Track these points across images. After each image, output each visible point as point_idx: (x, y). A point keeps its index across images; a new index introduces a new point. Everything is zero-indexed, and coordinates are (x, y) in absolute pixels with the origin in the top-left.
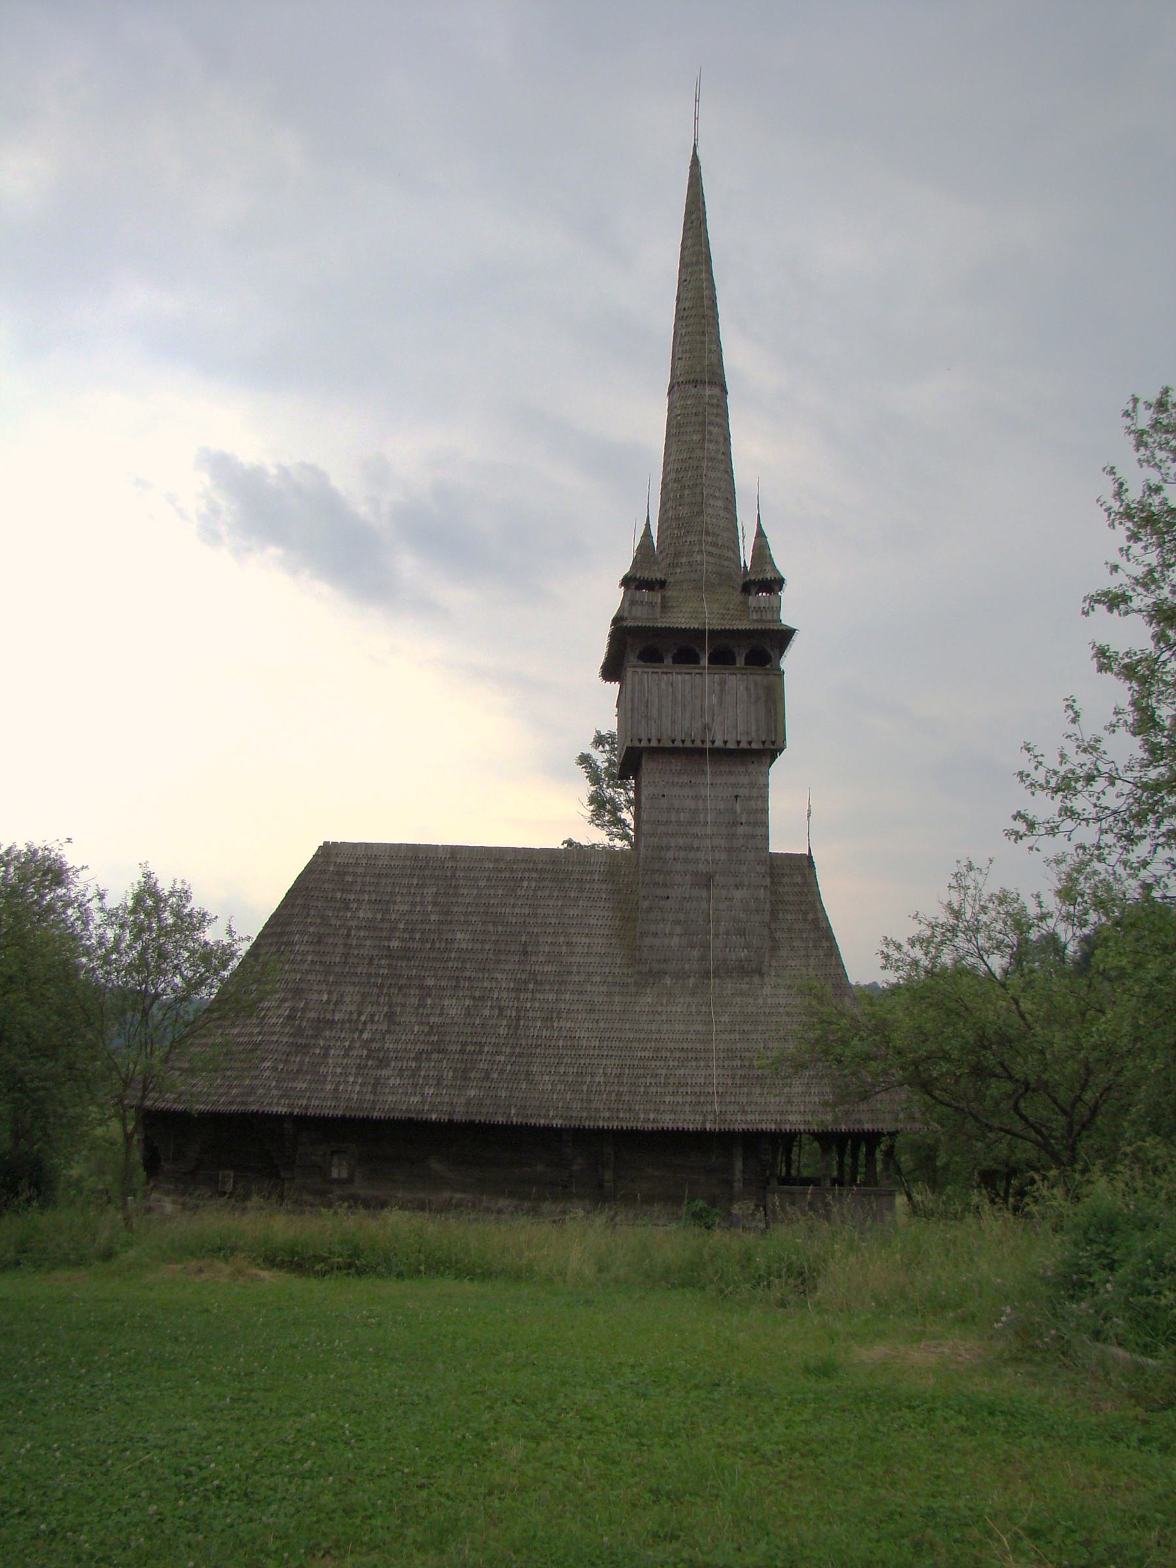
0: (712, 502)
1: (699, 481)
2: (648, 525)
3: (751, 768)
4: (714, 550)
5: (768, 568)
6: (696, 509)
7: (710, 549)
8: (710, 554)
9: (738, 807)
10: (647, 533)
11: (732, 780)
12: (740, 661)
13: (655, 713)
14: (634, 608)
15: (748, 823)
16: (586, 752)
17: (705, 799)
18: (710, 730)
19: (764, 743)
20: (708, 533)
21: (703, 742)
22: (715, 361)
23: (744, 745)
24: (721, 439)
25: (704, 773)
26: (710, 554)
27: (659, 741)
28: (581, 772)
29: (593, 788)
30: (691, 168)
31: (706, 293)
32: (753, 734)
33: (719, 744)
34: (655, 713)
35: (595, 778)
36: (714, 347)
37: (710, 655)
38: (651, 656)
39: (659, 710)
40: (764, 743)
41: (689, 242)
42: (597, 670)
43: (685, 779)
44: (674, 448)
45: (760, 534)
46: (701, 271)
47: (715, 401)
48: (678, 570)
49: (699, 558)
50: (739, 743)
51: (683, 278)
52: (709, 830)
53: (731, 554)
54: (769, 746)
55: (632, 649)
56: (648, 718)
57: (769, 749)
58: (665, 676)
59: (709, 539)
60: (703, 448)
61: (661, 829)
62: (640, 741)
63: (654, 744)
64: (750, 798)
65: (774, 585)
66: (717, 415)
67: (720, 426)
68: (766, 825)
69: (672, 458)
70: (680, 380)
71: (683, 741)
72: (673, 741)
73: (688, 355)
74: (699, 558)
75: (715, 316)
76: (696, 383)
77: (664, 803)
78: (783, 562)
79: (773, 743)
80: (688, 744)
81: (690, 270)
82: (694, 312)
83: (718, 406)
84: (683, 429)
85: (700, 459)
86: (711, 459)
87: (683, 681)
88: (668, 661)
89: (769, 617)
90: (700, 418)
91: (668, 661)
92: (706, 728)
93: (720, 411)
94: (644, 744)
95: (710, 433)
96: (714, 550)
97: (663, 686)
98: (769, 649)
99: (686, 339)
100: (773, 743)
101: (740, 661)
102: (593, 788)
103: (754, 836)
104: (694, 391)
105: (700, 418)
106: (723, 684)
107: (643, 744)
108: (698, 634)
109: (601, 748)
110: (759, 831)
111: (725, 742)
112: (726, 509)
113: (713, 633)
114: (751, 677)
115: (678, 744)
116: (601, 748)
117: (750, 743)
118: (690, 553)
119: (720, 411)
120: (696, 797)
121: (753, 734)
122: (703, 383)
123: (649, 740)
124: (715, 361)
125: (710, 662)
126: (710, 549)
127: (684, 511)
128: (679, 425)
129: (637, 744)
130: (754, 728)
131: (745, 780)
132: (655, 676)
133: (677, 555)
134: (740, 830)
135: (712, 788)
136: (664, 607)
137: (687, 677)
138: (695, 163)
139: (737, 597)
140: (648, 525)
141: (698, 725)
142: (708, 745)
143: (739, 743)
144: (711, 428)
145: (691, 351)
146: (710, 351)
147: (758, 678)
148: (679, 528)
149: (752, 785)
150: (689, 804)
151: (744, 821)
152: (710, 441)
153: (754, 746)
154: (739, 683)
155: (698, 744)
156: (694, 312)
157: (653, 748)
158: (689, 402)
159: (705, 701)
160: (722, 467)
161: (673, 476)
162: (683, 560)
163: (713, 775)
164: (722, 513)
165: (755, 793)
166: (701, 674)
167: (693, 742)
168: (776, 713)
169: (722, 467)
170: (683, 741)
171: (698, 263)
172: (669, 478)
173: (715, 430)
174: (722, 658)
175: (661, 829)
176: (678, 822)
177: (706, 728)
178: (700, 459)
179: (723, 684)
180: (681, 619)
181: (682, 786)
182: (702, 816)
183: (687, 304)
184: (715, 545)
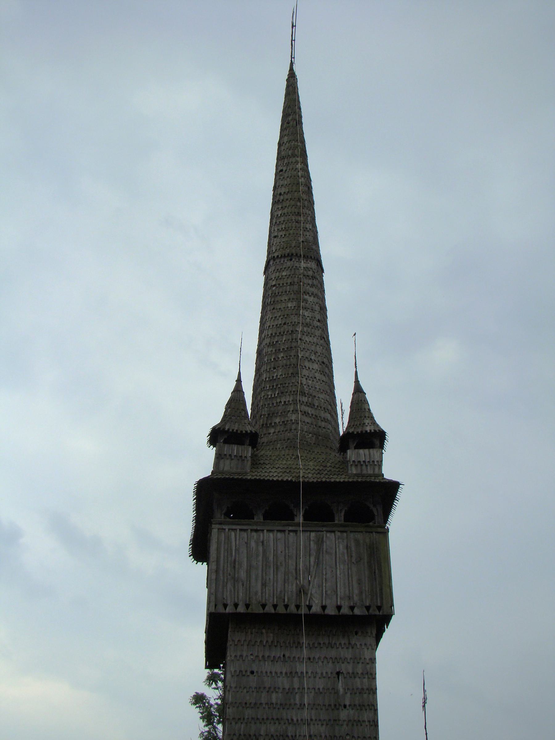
0: (307, 364)
1: (294, 344)
2: (239, 381)
3: (354, 640)
4: (309, 410)
5: (367, 421)
6: (291, 371)
7: (307, 409)
8: (305, 413)
9: (340, 686)
10: (238, 390)
11: (333, 653)
12: (339, 518)
13: (243, 575)
14: (222, 462)
15: (353, 706)
16: (200, 691)
17: (301, 676)
18: (306, 594)
19: (368, 608)
20: (303, 394)
21: (298, 607)
22: (311, 239)
23: (345, 611)
24: (317, 308)
25: (299, 645)
26: (305, 413)
27: (247, 606)
28: (195, 712)
29: (207, 729)
30: (288, 80)
31: (302, 180)
32: (356, 598)
33: (316, 609)
34: (243, 575)
35: (208, 718)
36: (309, 226)
37: (304, 516)
38: (241, 513)
39: (248, 572)
40: (368, 608)
41: (286, 139)
42: (206, 439)
43: (277, 653)
44: (269, 315)
45: (358, 390)
46: (297, 162)
47: (310, 273)
48: (272, 431)
49: (293, 417)
50: (339, 608)
51: (280, 168)
52: (305, 714)
53: (328, 416)
54: (374, 612)
55: (221, 506)
56: (235, 580)
57: (375, 618)
58: (254, 534)
59: (305, 399)
60: (298, 314)
61: (249, 713)
62: (225, 606)
63: (241, 609)
64: (354, 675)
65: (375, 439)
66: (312, 286)
67: (316, 296)
68: (373, 707)
69: (268, 324)
70: (276, 255)
71: (275, 606)
72: (264, 606)
73: (283, 233)
74: (293, 417)
75: (311, 203)
76: (290, 256)
77: (253, 681)
78: (382, 415)
79: (379, 608)
80: (281, 610)
81: (286, 161)
82: (289, 196)
83: (313, 278)
84: (278, 298)
85: (295, 325)
86: (308, 325)
87: (276, 540)
88: (259, 518)
89: (370, 472)
90: (296, 287)
91: (259, 518)
92: (302, 591)
93: (315, 282)
94: (230, 609)
95: (306, 301)
96: (309, 410)
97: (253, 544)
98: (371, 507)
99: (282, 219)
100: (379, 608)
101: (339, 518)
102: (207, 729)
103: (359, 722)
104: (289, 264)
105: (296, 287)
106: (320, 542)
107: (229, 610)
108: (290, 487)
109: (214, 685)
110: (366, 716)
111: (324, 608)
112: (322, 372)
113: (308, 485)
114: (352, 535)
115: (269, 609)
116: (214, 685)
117: (352, 608)
118: (285, 413)
119: (315, 282)
120: (291, 674)
121: (356, 598)
122: (298, 256)
123: (236, 605)
124: (311, 239)
125: (305, 519)
126: (307, 409)
127: (278, 373)
128: (274, 295)
129: (221, 610)
130: (356, 591)
131: (347, 654)
132: (244, 535)
133: (271, 415)
134: (344, 714)
135: (310, 665)
136: (256, 462)
137: (279, 535)
138: (292, 77)
139: (335, 456)
140: (239, 381)
141: (292, 588)
142: (303, 611)
143: (339, 608)
144: (307, 297)
145: (286, 229)
146: (305, 229)
147: (359, 536)
148: (273, 389)
149: (356, 660)
150: (284, 682)
151: (347, 703)
152: (305, 308)
153: (357, 612)
154: (337, 543)
155: (292, 609)
156: (289, 196)
157: (240, 614)
158: (284, 274)
159: (300, 563)
160: (318, 333)
161: (267, 341)
162: (277, 420)
163: (311, 647)
164: (317, 375)
165: (360, 669)
166: (295, 531)
167: (286, 606)
168: (381, 576)
169: (318, 333)
170: (275, 606)
171: (294, 155)
172: (264, 343)
173: (311, 299)
174: (319, 516)
175: (249, 713)
176: (270, 704)
177: (302, 591)
178: (295, 325)
179: (320, 542)
180: (273, 473)
181: (274, 660)
182: (297, 696)
183: (283, 190)
184: (311, 405)
